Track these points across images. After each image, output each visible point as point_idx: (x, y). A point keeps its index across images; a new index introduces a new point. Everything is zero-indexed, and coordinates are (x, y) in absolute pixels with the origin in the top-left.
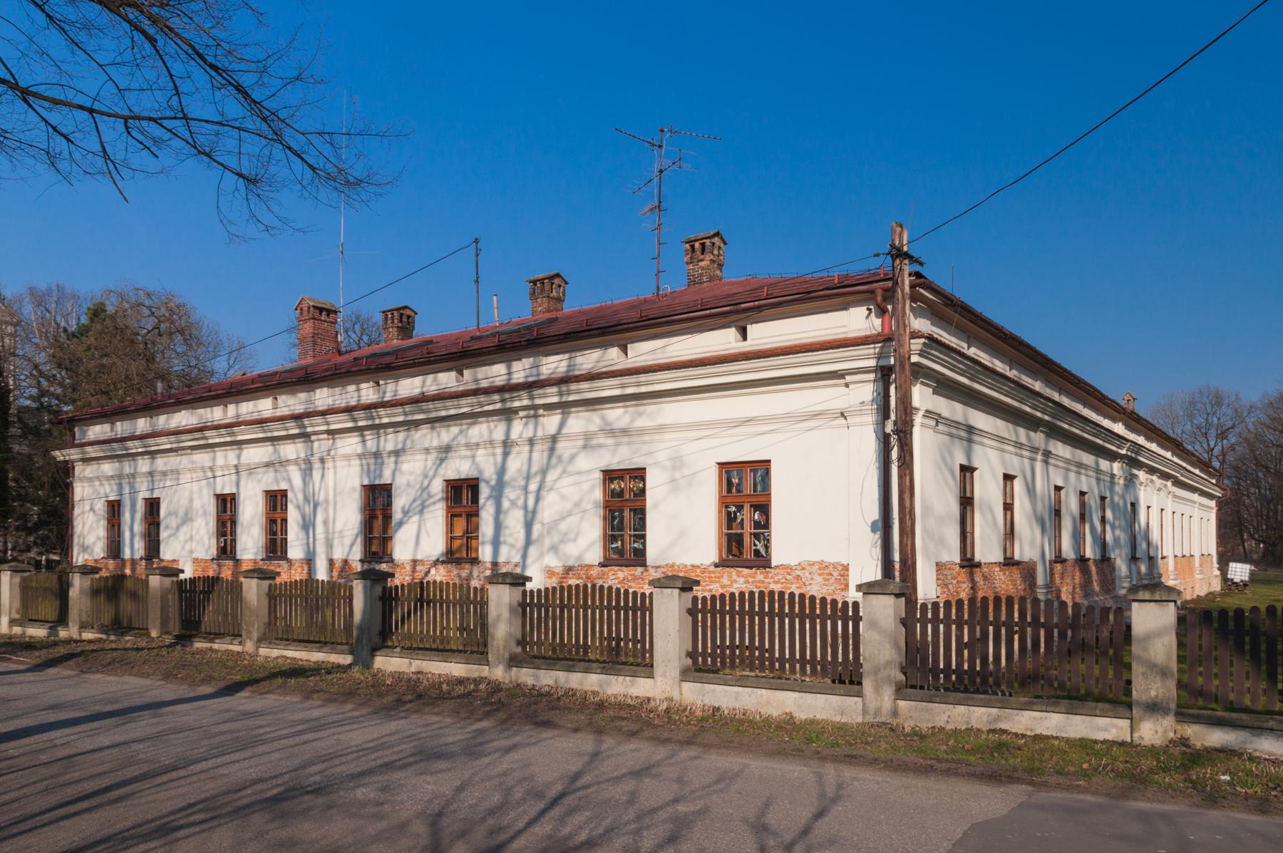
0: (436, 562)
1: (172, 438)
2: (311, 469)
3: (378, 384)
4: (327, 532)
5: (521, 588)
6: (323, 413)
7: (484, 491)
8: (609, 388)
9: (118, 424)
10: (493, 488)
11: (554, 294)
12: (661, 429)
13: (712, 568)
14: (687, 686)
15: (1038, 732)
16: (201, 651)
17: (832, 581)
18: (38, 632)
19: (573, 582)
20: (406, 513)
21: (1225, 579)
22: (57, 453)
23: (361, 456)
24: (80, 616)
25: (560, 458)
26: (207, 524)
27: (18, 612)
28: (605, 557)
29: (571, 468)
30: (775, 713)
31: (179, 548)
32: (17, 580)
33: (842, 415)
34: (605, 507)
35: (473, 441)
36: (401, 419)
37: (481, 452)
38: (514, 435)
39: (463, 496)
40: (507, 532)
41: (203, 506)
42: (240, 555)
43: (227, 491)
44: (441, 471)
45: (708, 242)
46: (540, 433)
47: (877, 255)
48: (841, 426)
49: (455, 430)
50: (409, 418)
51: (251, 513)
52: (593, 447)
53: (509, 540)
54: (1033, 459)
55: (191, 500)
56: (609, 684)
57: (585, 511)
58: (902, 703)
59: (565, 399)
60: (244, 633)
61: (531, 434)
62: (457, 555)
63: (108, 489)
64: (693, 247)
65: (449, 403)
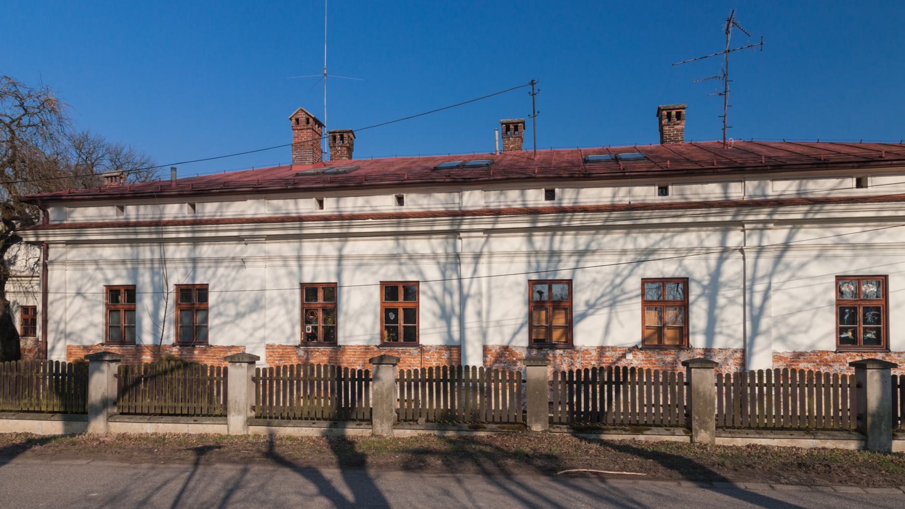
7: (695, 290)
8: (838, 211)
19: (802, 365)
26: (288, 312)
29: (800, 274)
42: (342, 338)
43: (322, 279)
52: (827, 258)
53: (726, 331)
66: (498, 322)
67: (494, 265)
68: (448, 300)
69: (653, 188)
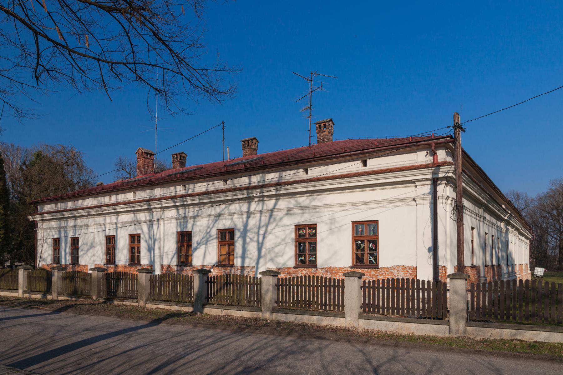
0: (213, 266)
1: (86, 210)
2: (152, 224)
3: (185, 186)
4: (160, 253)
5: (277, 278)
6: (160, 199)
7: (237, 235)
8: (300, 188)
9: (59, 204)
10: (241, 233)
11: (253, 147)
12: (325, 206)
13: (349, 269)
14: (361, 321)
15: (535, 340)
16: (118, 306)
17: (408, 274)
18: (37, 296)
20: (199, 244)
21: (533, 275)
22: (30, 217)
23: (176, 219)
24: (57, 289)
25: (275, 219)
26: (102, 249)
27: (26, 287)
28: (296, 264)
29: (280, 224)
30: (405, 333)
31: (88, 259)
32: (26, 273)
33: (414, 200)
34: (296, 241)
35: (232, 211)
36: (197, 202)
37: (235, 217)
38: (252, 209)
39: (226, 237)
40: (249, 252)
41: (100, 241)
43: (111, 234)
44: (216, 225)
45: (327, 124)
46: (265, 208)
47: (449, 127)
48: (413, 205)
49: (223, 207)
50: (201, 201)
51: (123, 243)
52: (291, 214)
53: (250, 256)
54: (480, 221)
55: (94, 238)
56: (322, 321)
57: (287, 243)
58: (468, 328)
59: (278, 193)
60: (139, 297)
61: (260, 208)
62: (223, 263)
63: (54, 233)
64: (320, 126)
65: (221, 195)
66: (167, 252)
67: (166, 225)
68: (150, 242)
69: (358, 162)
